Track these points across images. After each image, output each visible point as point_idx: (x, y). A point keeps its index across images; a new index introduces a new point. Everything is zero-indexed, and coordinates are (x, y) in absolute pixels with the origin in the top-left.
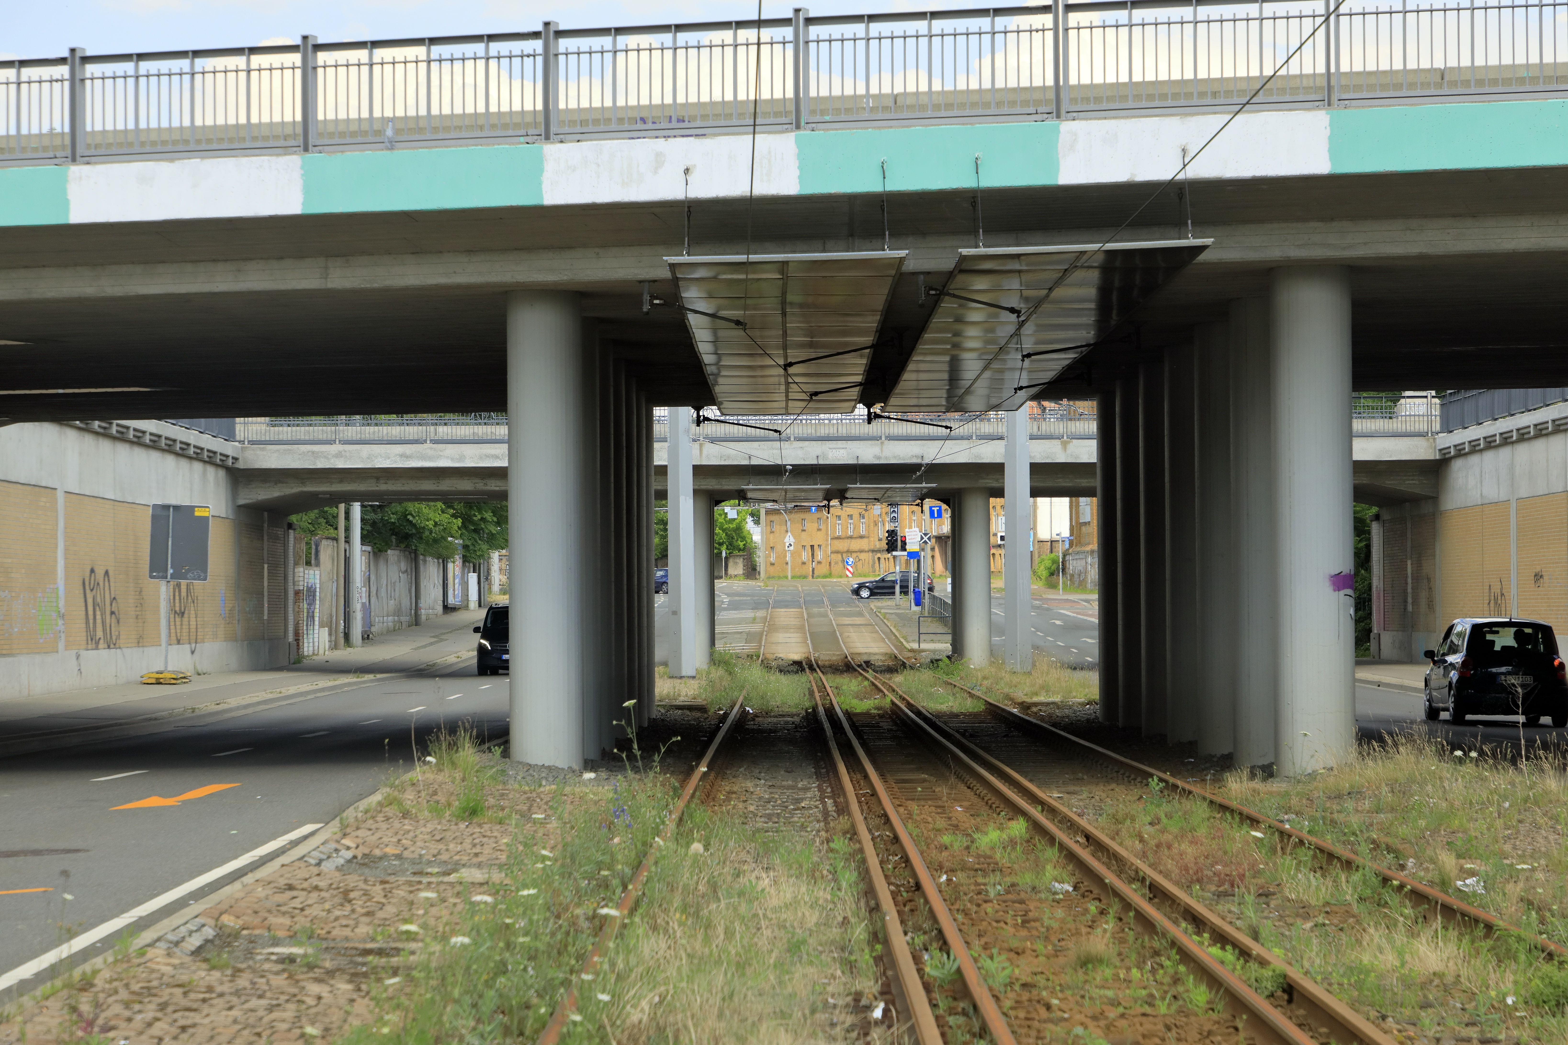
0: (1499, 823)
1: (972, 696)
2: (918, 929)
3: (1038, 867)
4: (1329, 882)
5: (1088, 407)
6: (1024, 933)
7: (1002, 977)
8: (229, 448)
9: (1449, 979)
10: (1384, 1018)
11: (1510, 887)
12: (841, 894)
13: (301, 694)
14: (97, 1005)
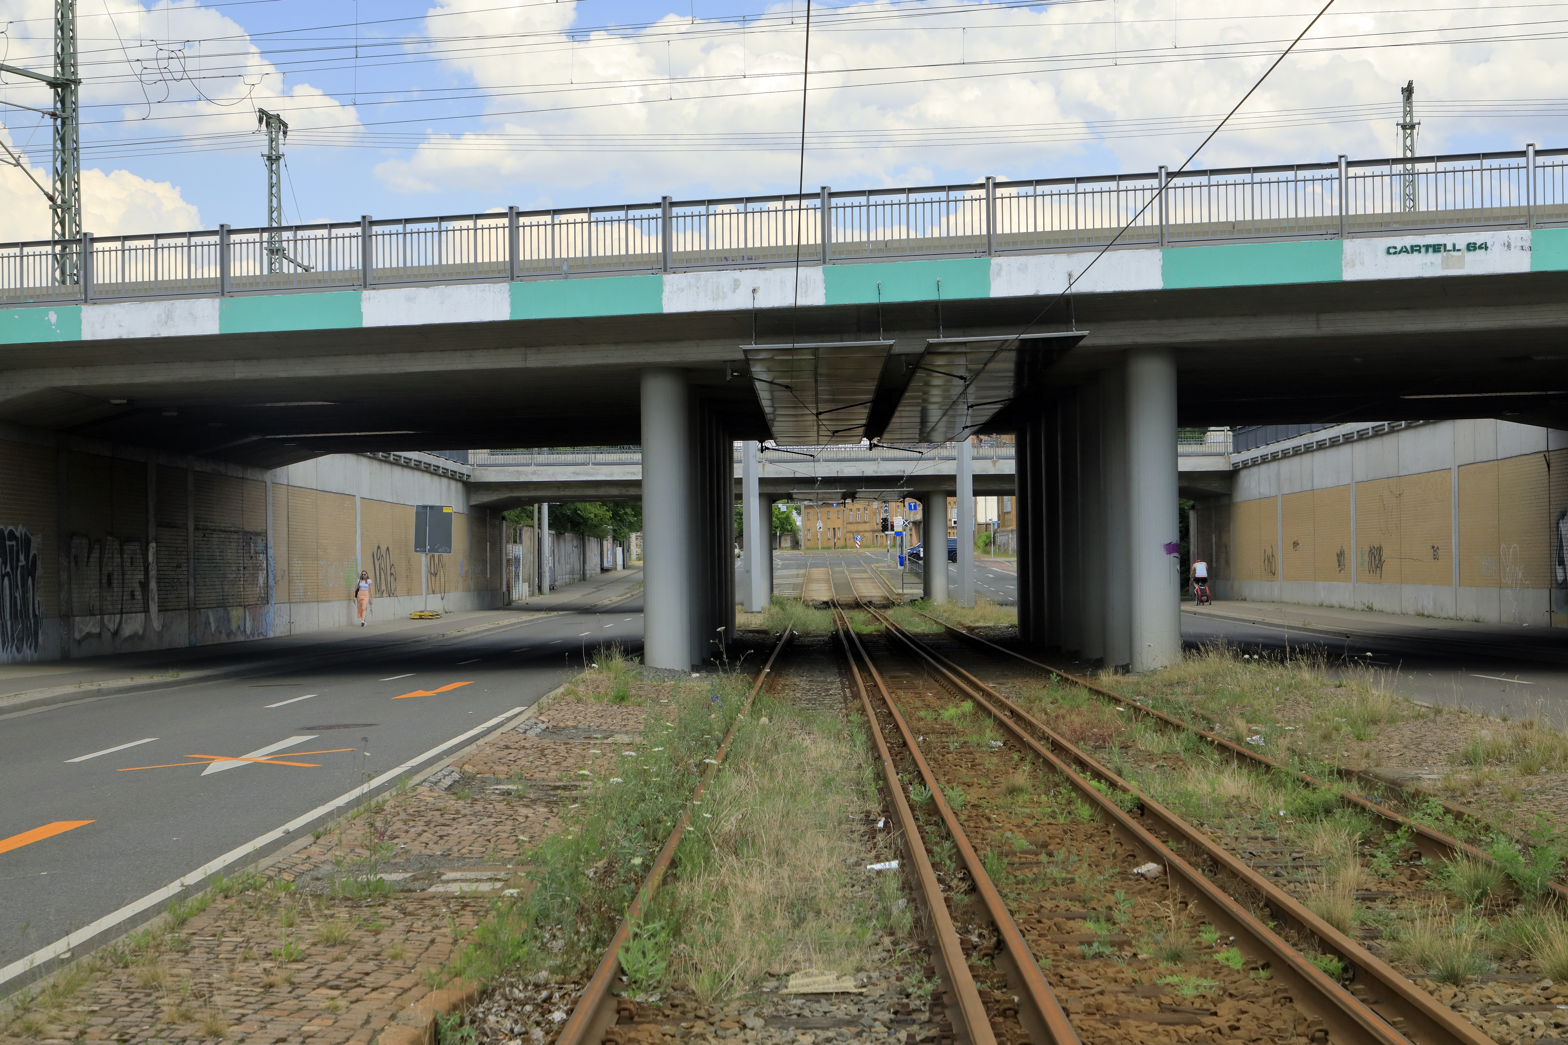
0: (1273, 701)
1: (936, 622)
2: (905, 770)
3: (981, 732)
4: (1166, 739)
5: (1009, 439)
6: (973, 773)
7: (959, 801)
8: (464, 469)
9: (1243, 800)
10: (1202, 825)
11: (1281, 741)
12: (856, 749)
13: (512, 625)
14: (387, 823)
